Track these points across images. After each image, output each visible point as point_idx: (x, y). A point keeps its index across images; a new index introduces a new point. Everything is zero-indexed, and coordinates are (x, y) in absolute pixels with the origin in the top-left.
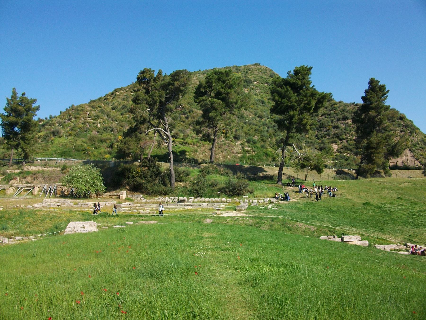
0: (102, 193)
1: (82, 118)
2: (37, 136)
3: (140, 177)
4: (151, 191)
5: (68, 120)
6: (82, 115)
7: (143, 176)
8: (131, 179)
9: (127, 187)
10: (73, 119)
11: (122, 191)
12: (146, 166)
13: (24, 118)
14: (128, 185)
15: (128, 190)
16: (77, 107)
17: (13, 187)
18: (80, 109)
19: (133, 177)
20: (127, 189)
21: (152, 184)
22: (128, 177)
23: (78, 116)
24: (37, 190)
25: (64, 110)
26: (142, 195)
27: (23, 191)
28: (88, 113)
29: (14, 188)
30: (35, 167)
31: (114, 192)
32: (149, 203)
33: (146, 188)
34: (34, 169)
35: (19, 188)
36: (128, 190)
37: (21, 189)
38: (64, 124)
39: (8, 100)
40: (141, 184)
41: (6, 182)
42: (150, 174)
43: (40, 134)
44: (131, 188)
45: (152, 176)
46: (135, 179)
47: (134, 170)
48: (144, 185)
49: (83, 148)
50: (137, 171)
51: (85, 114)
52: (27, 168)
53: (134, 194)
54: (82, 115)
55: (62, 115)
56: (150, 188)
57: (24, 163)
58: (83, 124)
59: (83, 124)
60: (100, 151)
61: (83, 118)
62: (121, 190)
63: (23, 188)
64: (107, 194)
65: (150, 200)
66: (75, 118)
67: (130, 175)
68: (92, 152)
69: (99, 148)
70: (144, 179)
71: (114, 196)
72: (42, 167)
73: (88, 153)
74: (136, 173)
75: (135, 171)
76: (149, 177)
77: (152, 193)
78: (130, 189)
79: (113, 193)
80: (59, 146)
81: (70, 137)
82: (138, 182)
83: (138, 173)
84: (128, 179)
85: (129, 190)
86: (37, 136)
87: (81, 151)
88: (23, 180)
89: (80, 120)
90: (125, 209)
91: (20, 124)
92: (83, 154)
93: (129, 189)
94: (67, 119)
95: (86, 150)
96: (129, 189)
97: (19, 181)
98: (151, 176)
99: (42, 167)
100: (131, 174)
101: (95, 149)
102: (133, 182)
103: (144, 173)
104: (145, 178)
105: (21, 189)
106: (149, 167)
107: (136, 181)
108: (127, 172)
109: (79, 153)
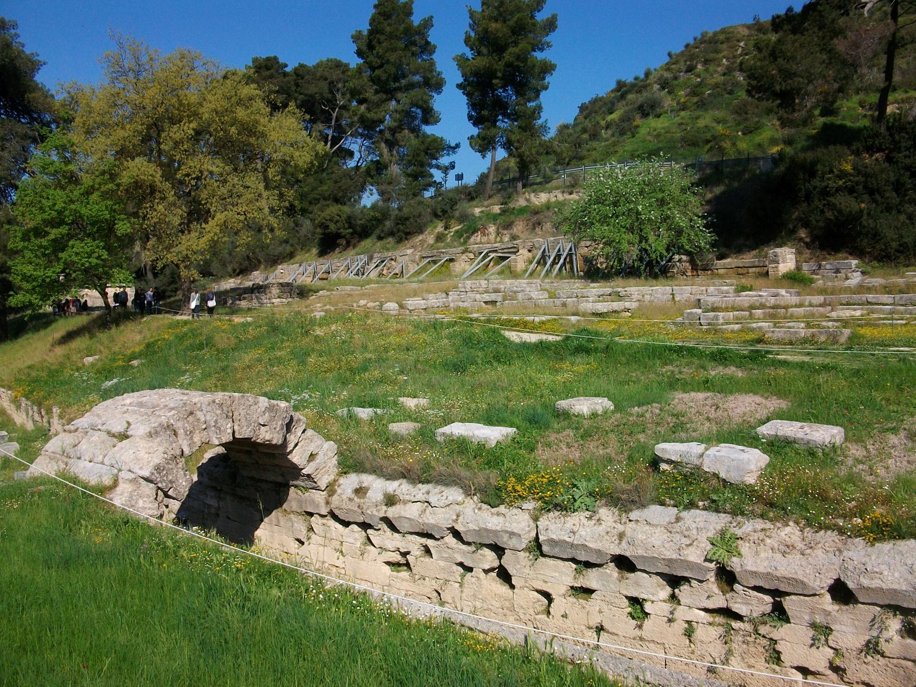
0: (712, 260)
1: (724, 60)
2: (603, 123)
3: (851, 191)
4: (894, 245)
5: (687, 72)
6: (725, 53)
7: (865, 187)
8: (816, 202)
9: (802, 233)
10: (699, 66)
11: (778, 250)
12: (880, 150)
13: (509, 54)
14: (806, 225)
15: (806, 243)
16: (715, 34)
17: (470, 252)
18: (722, 37)
19: (825, 193)
20: (801, 239)
21: (902, 217)
22: (808, 198)
23: (712, 56)
24: (525, 258)
25: (678, 49)
26: (854, 262)
27: (492, 264)
28: (742, 44)
29: (472, 256)
30: (547, 195)
31: (754, 252)
32: (869, 290)
33: (876, 236)
34: (541, 198)
35: (481, 253)
36: (806, 243)
37: (487, 255)
38: (675, 82)
39: (472, 14)
40: (855, 218)
41: (462, 240)
42: (893, 179)
43: (610, 117)
44: (814, 238)
45: (903, 185)
46: (831, 199)
47: (827, 169)
48: (865, 223)
49: (708, 136)
50: (841, 171)
51: (734, 48)
52: (528, 200)
53: (824, 259)
54: (725, 53)
55: (674, 60)
56: (890, 234)
57: (520, 185)
58: (724, 74)
59: (724, 74)
60: (757, 139)
61: (728, 59)
62: (780, 246)
63: (492, 255)
64: (728, 260)
65: (877, 281)
66: (706, 62)
67: (815, 188)
68: (734, 144)
69: (756, 129)
70: (866, 197)
71: (751, 270)
72: (563, 192)
73: (720, 147)
74: (837, 176)
75: (831, 172)
76: (890, 188)
77: (898, 251)
78: (813, 241)
79: (748, 259)
80: (649, 138)
81: (683, 113)
82: (840, 212)
83: (843, 174)
84: (805, 204)
85: (808, 245)
86: (603, 123)
87: (701, 144)
88: (505, 232)
89: (719, 65)
90: (717, 318)
91: (499, 74)
92: (708, 151)
93: (808, 240)
94: (683, 68)
95: (714, 138)
96: (808, 240)
97: (492, 237)
98: (898, 187)
99: (563, 192)
100: (816, 182)
101: (744, 134)
102: (822, 212)
103: (866, 175)
104: (871, 192)
105: (487, 255)
106: (891, 151)
107: (832, 206)
108: (801, 176)
109: (695, 150)
